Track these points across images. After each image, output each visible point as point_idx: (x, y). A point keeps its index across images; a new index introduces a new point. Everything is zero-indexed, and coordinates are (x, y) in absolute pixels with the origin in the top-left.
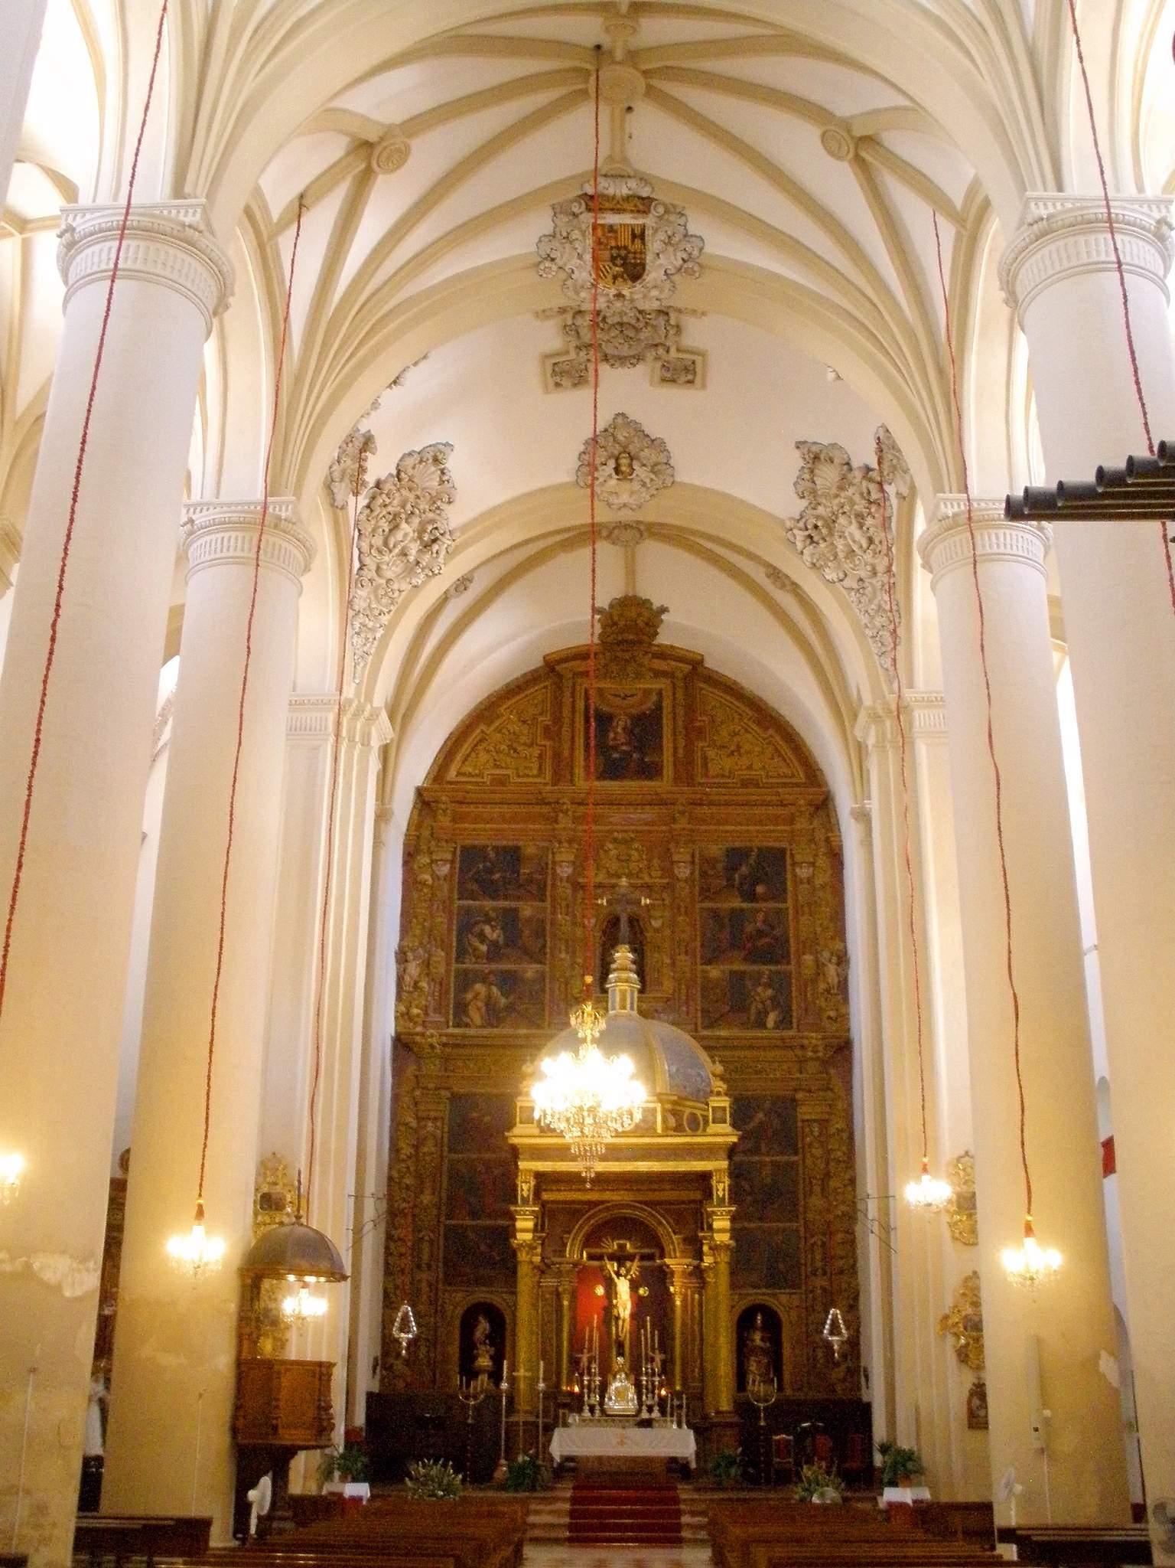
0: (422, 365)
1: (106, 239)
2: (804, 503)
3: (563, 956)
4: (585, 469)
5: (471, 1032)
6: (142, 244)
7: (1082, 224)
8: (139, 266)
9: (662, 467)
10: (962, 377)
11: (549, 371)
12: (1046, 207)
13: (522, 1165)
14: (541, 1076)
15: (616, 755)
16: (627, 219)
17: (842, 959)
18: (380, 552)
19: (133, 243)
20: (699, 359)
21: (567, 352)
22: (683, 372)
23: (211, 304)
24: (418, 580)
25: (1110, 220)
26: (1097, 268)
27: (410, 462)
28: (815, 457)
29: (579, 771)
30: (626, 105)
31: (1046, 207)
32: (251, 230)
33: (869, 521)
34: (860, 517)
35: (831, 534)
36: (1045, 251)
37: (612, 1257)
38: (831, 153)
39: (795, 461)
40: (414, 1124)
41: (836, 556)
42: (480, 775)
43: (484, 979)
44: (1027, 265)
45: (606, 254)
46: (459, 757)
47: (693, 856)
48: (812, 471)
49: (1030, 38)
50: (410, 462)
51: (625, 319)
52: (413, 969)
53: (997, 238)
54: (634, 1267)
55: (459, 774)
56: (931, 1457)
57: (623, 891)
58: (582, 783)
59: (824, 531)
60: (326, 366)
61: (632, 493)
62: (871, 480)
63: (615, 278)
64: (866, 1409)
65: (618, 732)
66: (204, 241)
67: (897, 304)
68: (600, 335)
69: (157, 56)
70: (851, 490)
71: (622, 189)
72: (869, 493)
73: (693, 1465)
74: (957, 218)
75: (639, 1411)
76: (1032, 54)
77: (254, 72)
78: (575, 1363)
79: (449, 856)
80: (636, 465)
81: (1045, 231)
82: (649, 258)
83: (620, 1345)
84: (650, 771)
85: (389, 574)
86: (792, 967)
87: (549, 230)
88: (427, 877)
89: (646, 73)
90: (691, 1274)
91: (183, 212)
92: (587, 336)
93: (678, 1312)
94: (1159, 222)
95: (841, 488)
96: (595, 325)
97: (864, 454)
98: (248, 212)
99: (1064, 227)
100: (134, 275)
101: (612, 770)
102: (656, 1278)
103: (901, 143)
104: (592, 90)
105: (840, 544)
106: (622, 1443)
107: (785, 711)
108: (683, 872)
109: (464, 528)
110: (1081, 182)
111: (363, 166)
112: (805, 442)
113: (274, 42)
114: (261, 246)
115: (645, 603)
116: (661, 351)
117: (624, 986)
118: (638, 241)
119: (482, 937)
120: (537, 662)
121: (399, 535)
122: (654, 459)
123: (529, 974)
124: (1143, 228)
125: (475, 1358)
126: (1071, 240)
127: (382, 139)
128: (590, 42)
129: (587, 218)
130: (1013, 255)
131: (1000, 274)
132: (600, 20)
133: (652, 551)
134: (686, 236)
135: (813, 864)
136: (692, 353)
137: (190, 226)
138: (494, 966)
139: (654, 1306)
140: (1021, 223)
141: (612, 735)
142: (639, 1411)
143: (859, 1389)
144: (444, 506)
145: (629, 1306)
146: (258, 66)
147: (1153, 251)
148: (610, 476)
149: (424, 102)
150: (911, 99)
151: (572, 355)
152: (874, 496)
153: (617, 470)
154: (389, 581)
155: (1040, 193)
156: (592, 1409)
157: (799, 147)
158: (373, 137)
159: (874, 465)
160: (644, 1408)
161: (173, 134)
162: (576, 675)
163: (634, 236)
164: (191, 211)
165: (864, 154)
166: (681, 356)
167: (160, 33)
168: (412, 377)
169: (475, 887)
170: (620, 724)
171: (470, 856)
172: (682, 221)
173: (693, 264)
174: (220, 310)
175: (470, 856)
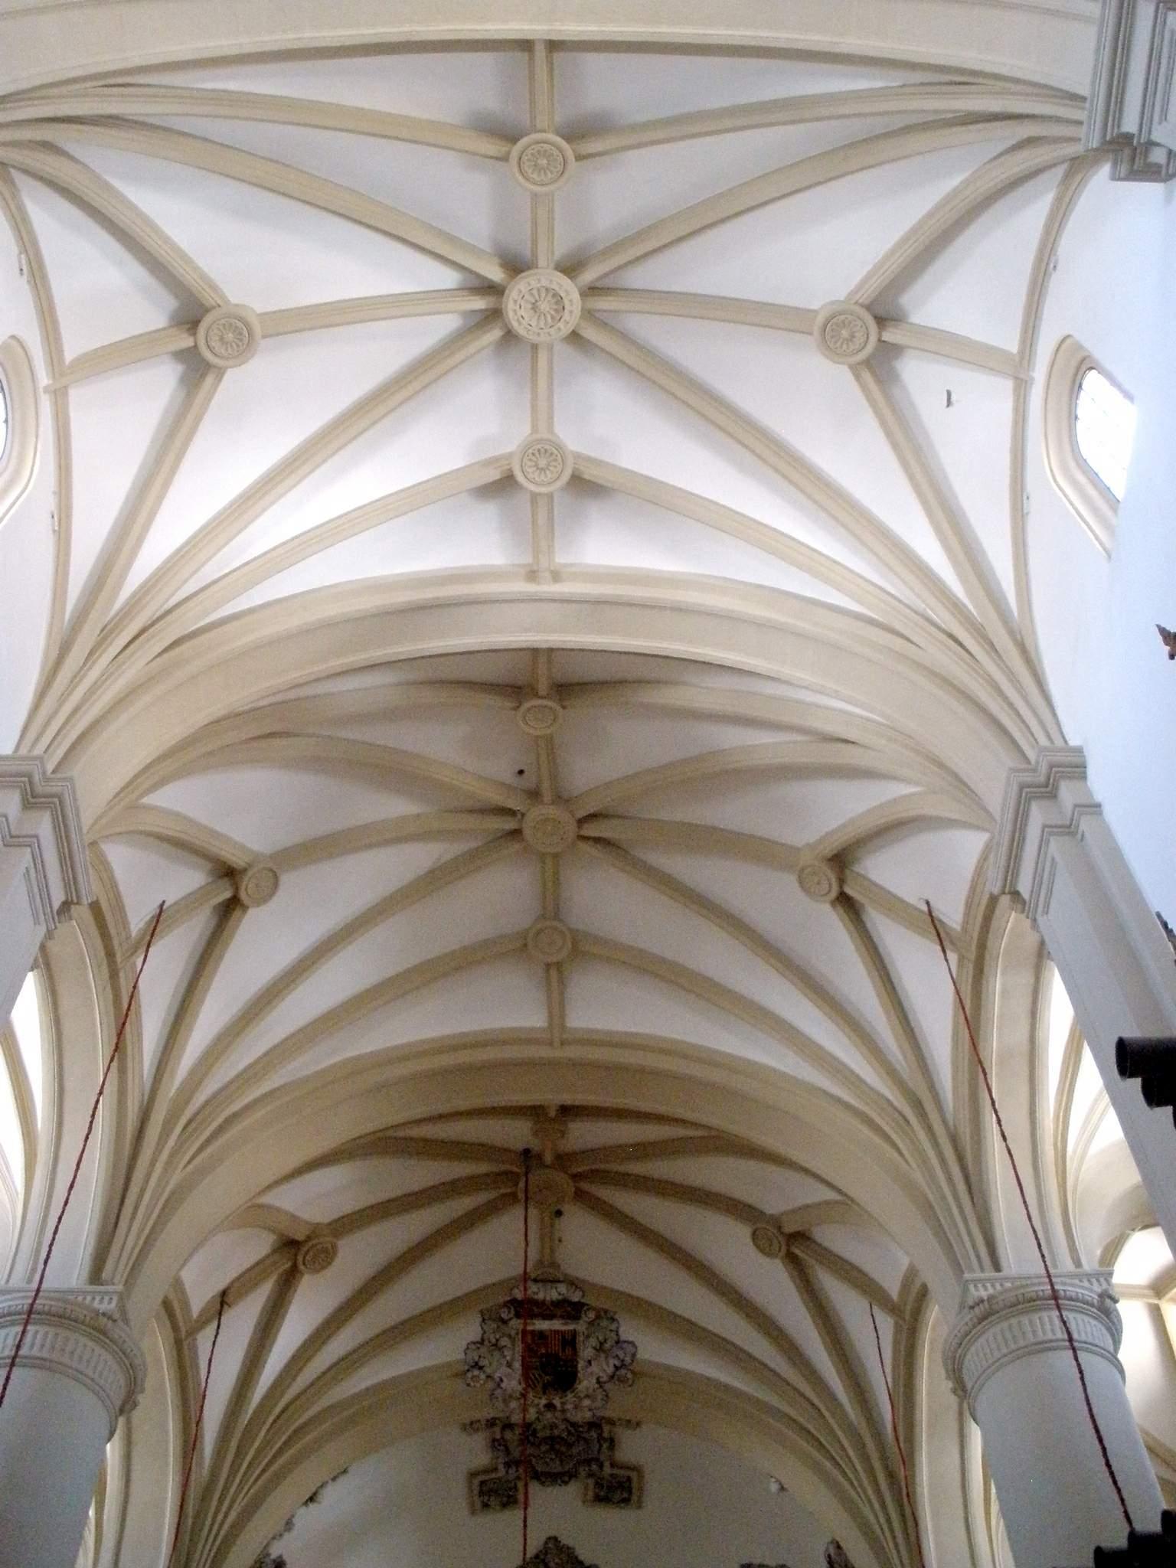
0: (342, 1480)
1: (13, 1324)
6: (52, 1331)
7: (1024, 1303)
8: (45, 1354)
10: (913, 1476)
12: (986, 1289)
16: (556, 1325)
19: (42, 1330)
20: (634, 1475)
21: (496, 1470)
22: (618, 1489)
23: (118, 1403)
25: (1055, 1296)
26: (1044, 1347)
30: (554, 1208)
31: (986, 1289)
32: (168, 1323)
36: (990, 1334)
38: (762, 1250)
44: (973, 1349)
49: (951, 1123)
51: (556, 1432)
53: (937, 1326)
60: (237, 1480)
66: (117, 1332)
67: (832, 1397)
68: (530, 1450)
69: (87, 1138)
71: (552, 1294)
74: (893, 1309)
76: (954, 1140)
77: (181, 1166)
81: (987, 1313)
82: (581, 1364)
89: (576, 1177)
91: (98, 1298)
92: (516, 1453)
94: (1101, 1296)
96: (524, 1441)
98: (166, 1304)
99: (1006, 1307)
100: (39, 1364)
103: (833, 1237)
104: (521, 1195)
110: (1019, 1259)
111: (288, 1265)
113: (207, 1134)
114: (178, 1343)
116: (594, 1467)
124: (1087, 1303)
126: (1014, 1321)
127: (309, 1238)
128: (520, 1146)
129: (516, 1324)
130: (957, 1341)
131: (945, 1364)
132: (529, 1124)
134: (617, 1342)
136: (628, 1468)
137: (104, 1314)
140: (962, 1306)
146: (187, 1157)
147: (1100, 1326)
149: (349, 1204)
150: (839, 1191)
151: (502, 1471)
155: (978, 1275)
157: (729, 1246)
158: (299, 1236)
161: (95, 1224)
164: (107, 1298)
165: (797, 1251)
166: (615, 1471)
167: (93, 1116)
168: (329, 1495)
172: (613, 1326)
173: (627, 1371)
174: (128, 1407)
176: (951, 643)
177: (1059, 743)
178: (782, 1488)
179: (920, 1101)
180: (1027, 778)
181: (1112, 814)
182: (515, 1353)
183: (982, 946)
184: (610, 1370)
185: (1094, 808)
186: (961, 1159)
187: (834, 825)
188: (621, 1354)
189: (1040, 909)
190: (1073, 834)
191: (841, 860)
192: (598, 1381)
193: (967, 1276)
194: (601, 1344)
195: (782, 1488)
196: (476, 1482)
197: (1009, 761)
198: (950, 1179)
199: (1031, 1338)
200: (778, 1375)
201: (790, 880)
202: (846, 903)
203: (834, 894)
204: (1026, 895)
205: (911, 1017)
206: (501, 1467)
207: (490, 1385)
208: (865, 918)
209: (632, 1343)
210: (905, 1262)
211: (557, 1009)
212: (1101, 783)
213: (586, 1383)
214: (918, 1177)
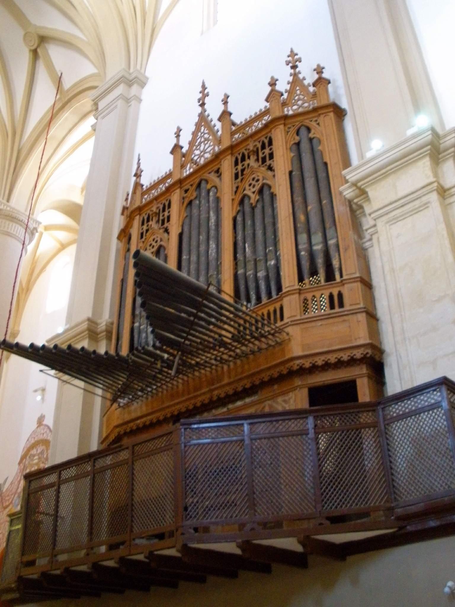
49: (22, 144)
76: (19, 152)
120: (350, 559)
176: (133, 10)
177: (143, 71)
179: (16, 131)
180: (127, 76)
181: (144, 106)
187: (49, 26)
189: (102, 115)
190: (128, 103)
191: (43, 39)
197: (124, 65)
199: (6, 229)
201: (22, 33)
202: (35, 53)
203: (33, 48)
204: (100, 109)
208: (37, 62)
212: (146, 93)
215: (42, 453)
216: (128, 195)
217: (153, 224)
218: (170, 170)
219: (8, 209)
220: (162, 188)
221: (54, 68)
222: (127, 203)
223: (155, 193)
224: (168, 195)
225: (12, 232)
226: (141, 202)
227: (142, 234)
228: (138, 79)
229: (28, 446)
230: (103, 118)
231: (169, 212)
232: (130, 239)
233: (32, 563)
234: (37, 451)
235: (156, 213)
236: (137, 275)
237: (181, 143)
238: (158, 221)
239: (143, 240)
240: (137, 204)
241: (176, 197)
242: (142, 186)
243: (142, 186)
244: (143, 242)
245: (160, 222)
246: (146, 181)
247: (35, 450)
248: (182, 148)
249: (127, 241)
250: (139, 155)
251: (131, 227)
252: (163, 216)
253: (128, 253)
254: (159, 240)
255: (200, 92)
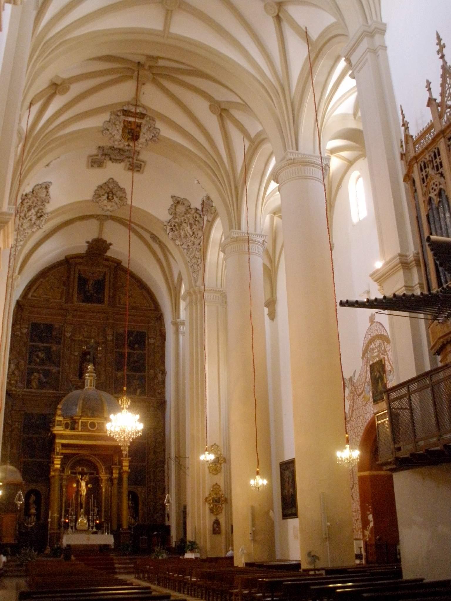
2: (171, 217)
3: (66, 365)
4: (96, 196)
5: (33, 390)
9: (123, 199)
11: (90, 161)
13: (57, 441)
14: (110, 421)
15: (89, 294)
17: (164, 373)
18: (23, 219)
20: (142, 164)
21: (97, 156)
22: (136, 167)
24: (34, 230)
27: (37, 187)
28: (178, 202)
29: (75, 299)
33: (194, 227)
34: (191, 224)
35: (180, 229)
37: (80, 473)
38: (212, 111)
39: (171, 202)
40: (10, 423)
41: (180, 236)
42: (40, 297)
43: (38, 372)
45: (127, 131)
46: (33, 290)
47: (114, 332)
48: (176, 206)
50: (37, 187)
52: (13, 366)
54: (87, 477)
55: (32, 296)
56: (200, 543)
57: (92, 344)
58: (76, 303)
59: (177, 228)
61: (112, 206)
62: (197, 213)
63: (128, 139)
64: (169, 528)
65: (90, 286)
67: (223, 162)
70: (188, 215)
72: (196, 217)
73: (113, 547)
74: (251, 141)
75: (89, 528)
78: (67, 511)
79: (27, 326)
80: (115, 197)
82: (141, 134)
83: (81, 504)
84: (100, 301)
85: (25, 227)
86: (146, 374)
87: (108, 120)
88: (19, 333)
90: (108, 480)
93: (104, 493)
95: (185, 214)
97: (196, 204)
101: (87, 299)
102: (95, 481)
105: (182, 233)
106: (88, 540)
107: (149, 284)
108: (110, 338)
109: (52, 212)
112: (174, 196)
115: (105, 241)
117: (92, 378)
118: (138, 128)
119: (37, 356)
120: (63, 258)
121: (30, 213)
122: (121, 195)
123: (54, 371)
125: (29, 510)
127: (61, 84)
129: (122, 118)
133: (110, 225)
135: (154, 338)
138: (42, 367)
139: (94, 491)
141: (87, 287)
142: (89, 528)
143: (165, 521)
144: (46, 204)
145: (85, 491)
148: (105, 200)
152: (198, 219)
153: (108, 198)
154: (24, 229)
155: (291, 151)
156: (72, 528)
157: (200, 107)
158: (59, 82)
159: (200, 208)
160: (90, 528)
162: (76, 264)
163: (137, 126)
165: (222, 114)
169: (36, 338)
170: (91, 283)
171: (35, 326)
173: (156, 138)
175: (35, 326)
178: (199, 183)
179: (284, 87)
181: (390, 52)
182: (120, 127)
183: (321, 50)
184: (151, 137)
185: (384, 48)
186: (293, 110)
188: (155, 132)
192: (146, 140)
193: (288, 150)
194: (149, 128)
195: (199, 183)
196: (91, 158)
198: (288, 117)
200: (206, 150)
202: (278, 18)
203: (276, 14)
205: (288, 61)
206: (100, 156)
207: (110, 136)
209: (159, 129)
210: (260, 128)
211: (167, 24)
212: (389, 38)
213: (142, 140)
214: (278, 112)
215: (380, 346)
216: (402, 142)
217: (430, 170)
218: (431, 121)
219: (300, 156)
220: (429, 137)
221: (299, 26)
222: (403, 149)
223: (424, 143)
224: (435, 144)
225: (309, 175)
226: (415, 152)
227: (423, 179)
228: (378, 29)
229: (367, 342)
230: (359, 70)
231: (440, 159)
232: (414, 182)
233: (399, 449)
234: (375, 345)
235: (429, 161)
236: (435, 255)
237: (434, 97)
238: (433, 168)
239: (425, 184)
240: (412, 154)
241: (442, 145)
242: (412, 136)
243: (412, 136)
244: (426, 186)
245: (435, 168)
246: (414, 132)
247: (373, 345)
248: (435, 100)
249: (412, 183)
250: (401, 106)
251: (413, 172)
252: (436, 162)
253: (415, 194)
254: (438, 184)
255: (437, 44)
